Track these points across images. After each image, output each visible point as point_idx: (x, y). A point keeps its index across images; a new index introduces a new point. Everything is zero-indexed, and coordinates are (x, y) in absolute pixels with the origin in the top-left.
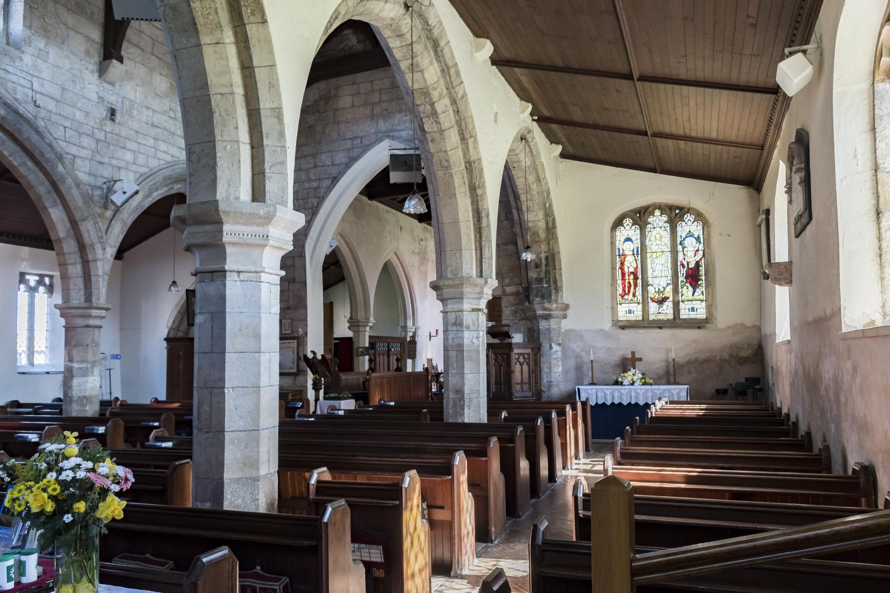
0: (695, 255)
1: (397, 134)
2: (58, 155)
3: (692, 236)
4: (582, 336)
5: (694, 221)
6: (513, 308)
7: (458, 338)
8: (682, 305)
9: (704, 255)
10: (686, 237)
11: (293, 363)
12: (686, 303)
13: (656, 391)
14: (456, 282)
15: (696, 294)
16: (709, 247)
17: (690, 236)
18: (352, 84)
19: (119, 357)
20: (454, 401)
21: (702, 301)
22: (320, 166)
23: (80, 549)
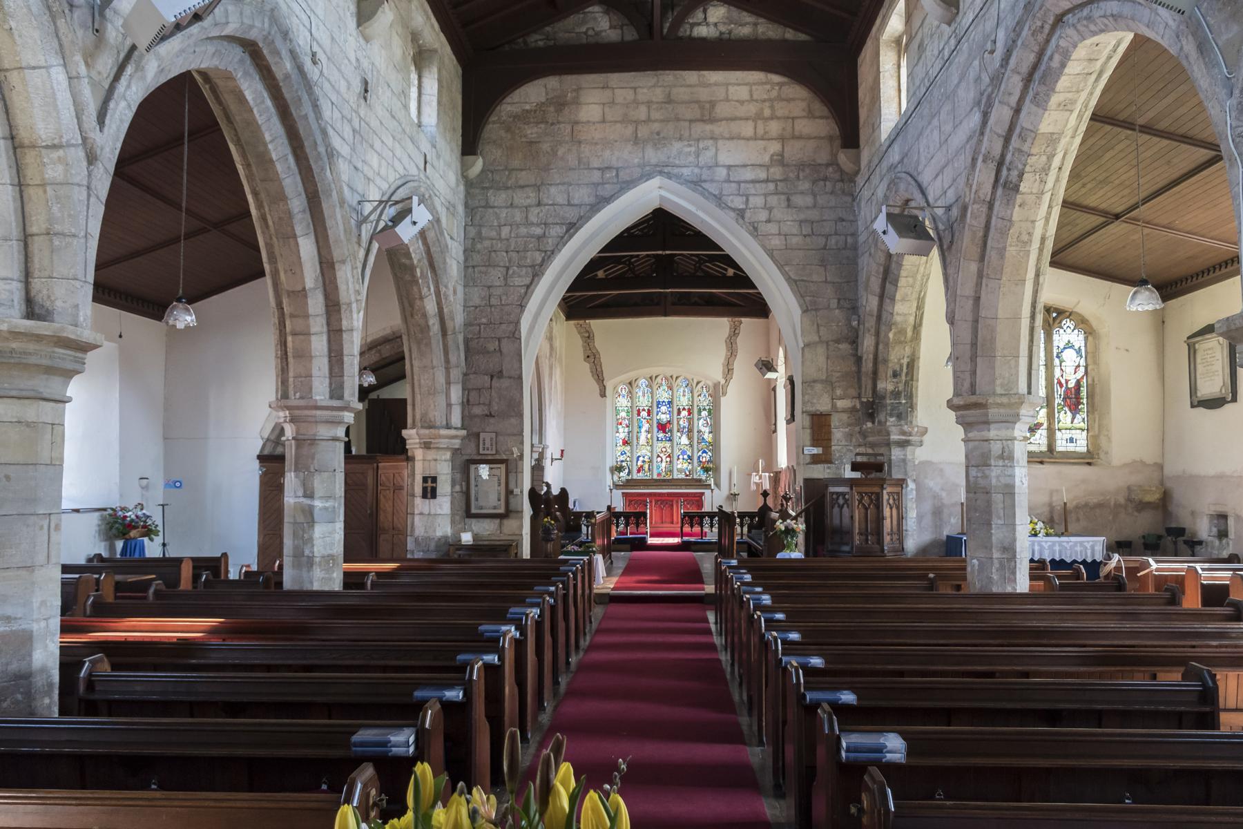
0: (1075, 373)
1: (676, 170)
2: (329, 149)
3: (1072, 347)
4: (941, 470)
5: (1074, 329)
6: (847, 430)
7: (1006, 476)
8: (1058, 434)
9: (1086, 372)
10: (1065, 348)
11: (499, 500)
12: (1063, 431)
13: (1065, 544)
14: (1013, 401)
15: (1076, 421)
16: (1096, 363)
17: (1069, 348)
18: (603, 88)
19: (178, 484)
20: (1001, 563)
21: (1083, 430)
22: (547, 205)
23: (1124, 802)
